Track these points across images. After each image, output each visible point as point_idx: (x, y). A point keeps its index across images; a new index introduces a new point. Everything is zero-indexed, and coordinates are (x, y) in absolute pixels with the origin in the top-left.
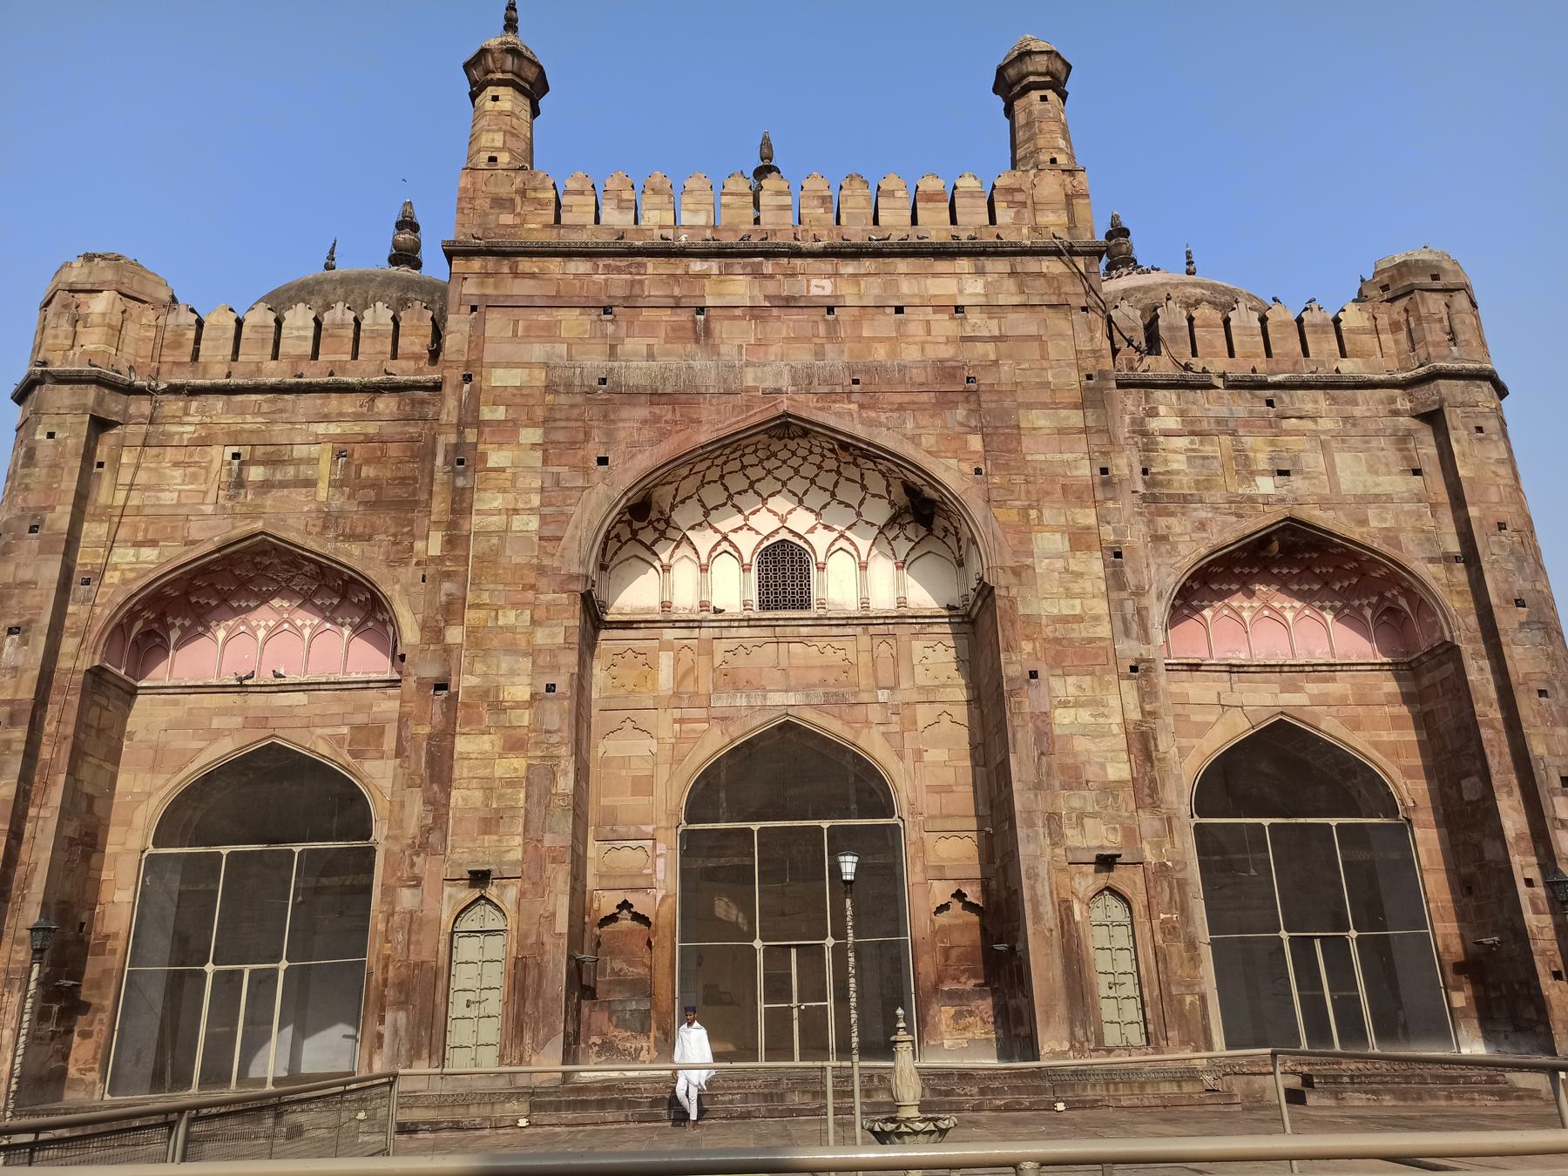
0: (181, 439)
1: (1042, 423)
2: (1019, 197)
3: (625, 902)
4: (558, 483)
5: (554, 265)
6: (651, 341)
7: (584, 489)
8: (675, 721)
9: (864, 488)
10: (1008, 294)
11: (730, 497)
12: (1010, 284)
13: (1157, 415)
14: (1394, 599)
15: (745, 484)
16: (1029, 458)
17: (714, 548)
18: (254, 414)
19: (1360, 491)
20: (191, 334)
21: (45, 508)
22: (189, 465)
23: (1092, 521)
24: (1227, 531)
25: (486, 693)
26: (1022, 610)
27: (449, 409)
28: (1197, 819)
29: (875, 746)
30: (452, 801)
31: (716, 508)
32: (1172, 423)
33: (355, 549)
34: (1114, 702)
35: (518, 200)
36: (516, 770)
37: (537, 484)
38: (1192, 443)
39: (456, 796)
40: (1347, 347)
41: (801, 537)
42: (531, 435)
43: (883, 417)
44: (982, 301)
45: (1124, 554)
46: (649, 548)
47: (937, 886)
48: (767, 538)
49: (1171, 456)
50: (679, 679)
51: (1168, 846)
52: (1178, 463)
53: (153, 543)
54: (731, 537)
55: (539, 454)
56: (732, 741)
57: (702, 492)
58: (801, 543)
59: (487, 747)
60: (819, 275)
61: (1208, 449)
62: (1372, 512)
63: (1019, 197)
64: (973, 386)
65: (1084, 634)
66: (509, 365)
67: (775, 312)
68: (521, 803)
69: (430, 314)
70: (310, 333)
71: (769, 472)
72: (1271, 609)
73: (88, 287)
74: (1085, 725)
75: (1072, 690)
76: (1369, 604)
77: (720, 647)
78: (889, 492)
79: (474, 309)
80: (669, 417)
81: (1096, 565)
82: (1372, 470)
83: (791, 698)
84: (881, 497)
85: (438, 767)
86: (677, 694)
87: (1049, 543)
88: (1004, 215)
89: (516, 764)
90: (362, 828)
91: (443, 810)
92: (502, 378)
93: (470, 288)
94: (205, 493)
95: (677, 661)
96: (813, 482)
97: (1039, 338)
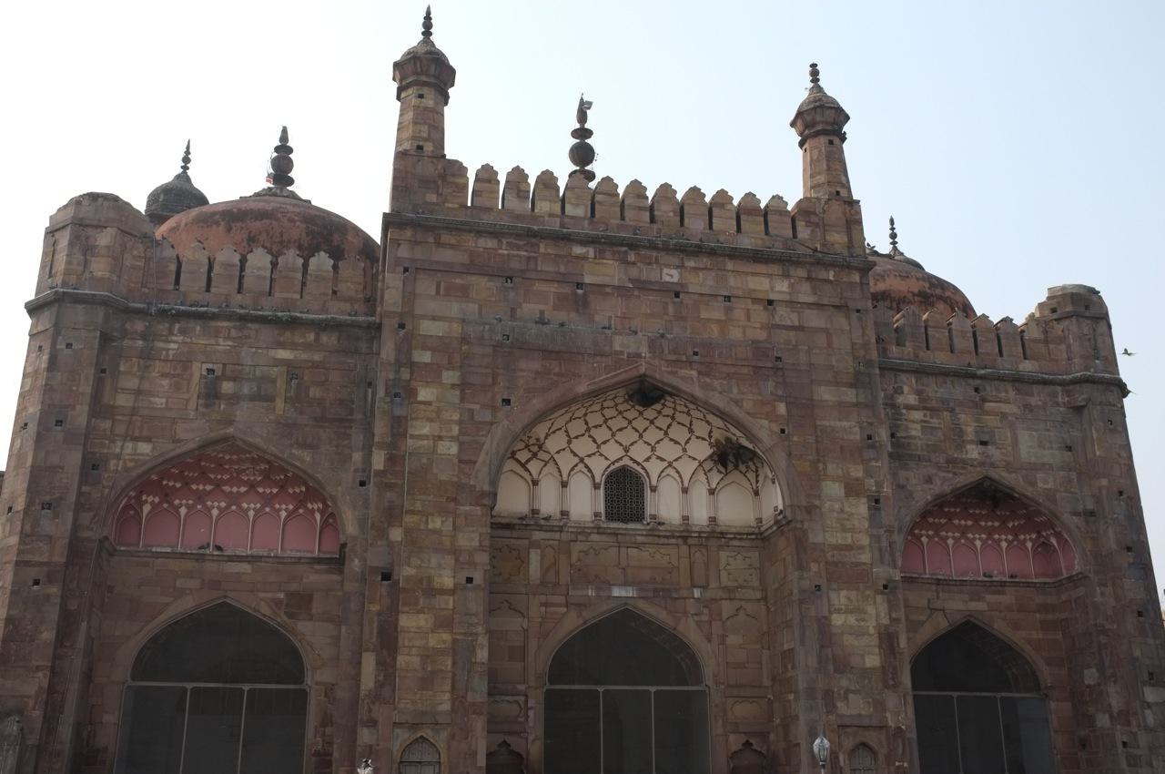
0: (167, 355)
1: (826, 397)
2: (814, 219)
4: (472, 417)
5: (471, 242)
6: (542, 307)
8: (542, 604)
9: (691, 431)
10: (806, 294)
11: (588, 430)
12: (806, 287)
13: (902, 393)
14: (1047, 538)
16: (818, 423)
17: (572, 469)
18: (225, 338)
19: (1033, 460)
20: (173, 267)
21: (67, 407)
22: (174, 376)
23: (860, 474)
24: (944, 483)
25: (421, 581)
27: (388, 349)
29: (691, 632)
30: (398, 663)
31: (576, 437)
32: (912, 399)
33: (307, 456)
34: (871, 610)
35: (440, 182)
36: (444, 642)
37: (456, 417)
38: (925, 415)
39: (401, 660)
40: (1028, 352)
42: (450, 377)
43: (716, 383)
44: (787, 297)
45: (881, 501)
46: (523, 465)
47: (732, 737)
50: (545, 572)
51: (903, 715)
52: (915, 431)
53: (148, 440)
54: (587, 460)
55: (457, 392)
56: (585, 623)
57: (569, 425)
58: (639, 469)
59: (422, 623)
60: (668, 266)
61: (935, 422)
62: (1040, 475)
63: (814, 219)
64: (780, 364)
65: (853, 560)
66: (434, 318)
67: (636, 293)
68: (449, 668)
71: (620, 413)
72: (967, 539)
73: (95, 223)
74: (851, 627)
75: (843, 600)
76: (1030, 539)
78: (710, 437)
79: (406, 270)
80: (557, 370)
81: (862, 508)
82: (1041, 446)
83: (629, 592)
84: (703, 439)
86: (543, 583)
87: (833, 489)
88: (804, 232)
90: (298, 676)
92: (429, 328)
93: (404, 252)
94: (187, 401)
95: (543, 556)
96: (652, 422)
97: (826, 331)
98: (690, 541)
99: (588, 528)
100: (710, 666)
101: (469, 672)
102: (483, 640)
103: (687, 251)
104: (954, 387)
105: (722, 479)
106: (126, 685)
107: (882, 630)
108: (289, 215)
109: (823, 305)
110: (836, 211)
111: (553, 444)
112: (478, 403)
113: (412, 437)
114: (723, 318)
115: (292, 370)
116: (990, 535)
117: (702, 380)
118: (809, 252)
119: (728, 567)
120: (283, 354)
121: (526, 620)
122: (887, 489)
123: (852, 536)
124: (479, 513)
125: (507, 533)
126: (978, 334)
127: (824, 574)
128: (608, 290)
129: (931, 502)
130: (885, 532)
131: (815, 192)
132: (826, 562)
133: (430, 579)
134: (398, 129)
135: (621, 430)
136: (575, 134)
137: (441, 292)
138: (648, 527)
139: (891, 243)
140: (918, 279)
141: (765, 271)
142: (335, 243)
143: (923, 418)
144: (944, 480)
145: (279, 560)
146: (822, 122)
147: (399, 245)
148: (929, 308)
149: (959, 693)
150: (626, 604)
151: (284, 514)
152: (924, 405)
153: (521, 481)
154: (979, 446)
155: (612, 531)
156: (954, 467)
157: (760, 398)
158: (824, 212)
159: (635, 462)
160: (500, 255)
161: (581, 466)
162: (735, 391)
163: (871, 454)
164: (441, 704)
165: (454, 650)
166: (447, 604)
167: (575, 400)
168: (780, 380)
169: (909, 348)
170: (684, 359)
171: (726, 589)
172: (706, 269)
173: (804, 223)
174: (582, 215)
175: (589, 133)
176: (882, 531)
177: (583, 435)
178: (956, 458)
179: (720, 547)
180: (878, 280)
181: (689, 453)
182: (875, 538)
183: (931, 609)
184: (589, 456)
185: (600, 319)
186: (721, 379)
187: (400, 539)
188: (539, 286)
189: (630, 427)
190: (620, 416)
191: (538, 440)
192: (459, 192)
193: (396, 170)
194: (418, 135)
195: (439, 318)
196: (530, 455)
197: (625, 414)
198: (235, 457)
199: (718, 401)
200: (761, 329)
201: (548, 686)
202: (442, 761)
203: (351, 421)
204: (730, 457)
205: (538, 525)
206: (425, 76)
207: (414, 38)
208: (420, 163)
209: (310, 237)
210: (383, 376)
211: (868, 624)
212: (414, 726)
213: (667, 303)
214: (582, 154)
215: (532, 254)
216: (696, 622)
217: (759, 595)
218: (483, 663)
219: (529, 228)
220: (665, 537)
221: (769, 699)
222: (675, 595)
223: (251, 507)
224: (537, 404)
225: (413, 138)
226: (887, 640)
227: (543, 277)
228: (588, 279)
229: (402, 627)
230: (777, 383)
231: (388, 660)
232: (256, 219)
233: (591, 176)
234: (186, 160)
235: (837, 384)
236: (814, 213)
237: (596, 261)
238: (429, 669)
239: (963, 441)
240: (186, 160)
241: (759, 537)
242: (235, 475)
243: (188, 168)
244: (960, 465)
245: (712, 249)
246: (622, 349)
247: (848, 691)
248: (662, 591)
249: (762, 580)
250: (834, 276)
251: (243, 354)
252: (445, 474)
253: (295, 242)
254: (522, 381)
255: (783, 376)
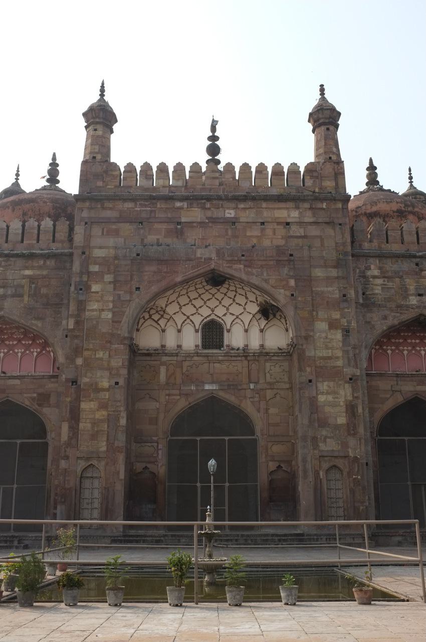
1: (319, 274)
2: (315, 174)
3: (146, 467)
6: (158, 237)
7: (130, 301)
8: (167, 395)
9: (247, 298)
10: (309, 217)
11: (191, 301)
13: (370, 269)
15: (197, 295)
17: (183, 322)
24: (394, 319)
25: (92, 385)
26: (307, 354)
27: (76, 266)
28: (379, 438)
29: (248, 407)
30: (80, 427)
31: (184, 305)
32: (376, 272)
33: (39, 324)
34: (342, 392)
35: (105, 175)
36: (104, 416)
37: (111, 299)
38: (384, 281)
39: (81, 425)
41: (220, 318)
42: (108, 278)
43: (254, 271)
44: (297, 220)
46: (156, 322)
47: (271, 464)
48: (206, 318)
49: (375, 287)
50: (168, 378)
51: (359, 450)
52: (378, 290)
54: (191, 317)
55: (112, 286)
56: (190, 404)
58: (220, 320)
60: (228, 208)
61: (390, 284)
63: (315, 174)
64: (292, 258)
65: (332, 365)
66: (100, 248)
67: (210, 225)
68: (106, 429)
69: (68, 222)
70: (20, 232)
71: (207, 291)
74: (330, 402)
75: (325, 387)
77: (186, 364)
78: (257, 301)
79: (86, 223)
80: (165, 270)
81: (338, 335)
84: (254, 302)
85: (75, 416)
86: (167, 384)
87: (322, 326)
89: (102, 414)
91: (76, 431)
92: (98, 253)
93: (85, 214)
95: (167, 370)
96: (225, 295)
97: (320, 237)
98: (249, 358)
99: (257, 353)
100: (259, 425)
101: (116, 431)
102: (124, 415)
103: (237, 199)
104: (403, 264)
105: (267, 323)
106: (168, 439)
107: (348, 403)
108: (43, 200)
109: (319, 223)
110: (329, 169)
111: (171, 310)
112: (122, 291)
113: (89, 310)
114: (259, 235)
115: (32, 279)
116: (414, 347)
117: (246, 270)
118: (311, 193)
119: (270, 372)
120: (28, 272)
121: (158, 403)
122: (354, 324)
123: (332, 351)
124: (123, 348)
125: (148, 358)
126: (419, 232)
127: (314, 373)
128: (195, 224)
129: (386, 331)
130: (352, 348)
131: (318, 159)
132: (316, 367)
133: (96, 384)
134: (85, 149)
135: (209, 300)
136: (210, 138)
137: (105, 233)
138: (225, 352)
139: (409, 182)
140: (397, 203)
141: (285, 207)
142: (69, 212)
143: (383, 283)
144: (394, 317)
145: (34, 377)
146: (323, 118)
147: (82, 210)
148: (403, 219)
149: (409, 438)
150: (212, 393)
151: (35, 354)
152: (384, 275)
153: (157, 331)
154: (418, 297)
155: (205, 355)
156: (400, 310)
157: (279, 277)
158: (321, 169)
159: (218, 317)
160: (135, 211)
161: (188, 321)
162: (265, 275)
163: (345, 305)
164: (102, 447)
165: (108, 419)
166: (105, 396)
167: (175, 285)
168: (292, 267)
169: (375, 243)
170: (236, 259)
171: (270, 383)
172: (250, 208)
173: (309, 177)
174: (181, 185)
175: (217, 138)
176: (350, 348)
177: (188, 304)
178: (403, 305)
179: (266, 361)
180: (373, 205)
181: (247, 310)
182: (346, 352)
183: (393, 391)
184: (192, 315)
185: (190, 241)
186: (257, 268)
187: (81, 364)
188: (156, 226)
189: (214, 298)
190: (207, 293)
191: (162, 308)
192: (114, 179)
193: (81, 171)
194: (93, 151)
195: (104, 247)
196: (160, 316)
197: (198, 290)
198: (8, 326)
199: (255, 280)
200: (282, 239)
201: (170, 437)
202: (102, 476)
203: (61, 304)
204: (268, 312)
205: (165, 353)
206: (101, 118)
207: (95, 98)
208: (94, 166)
209: (55, 210)
210: (75, 279)
211: (340, 400)
212: (88, 459)
213: (227, 229)
214: (214, 150)
215: (153, 209)
216: (251, 402)
217: (288, 386)
218: (123, 426)
219: (151, 195)
220: (234, 356)
221: (293, 443)
222: (240, 388)
223: (19, 351)
224: (154, 289)
225: (91, 153)
226: (351, 409)
227: (159, 221)
228: (183, 220)
229: (82, 409)
230: (291, 268)
231: (75, 426)
232: (27, 203)
233: (218, 162)
234: (17, 175)
235: (326, 266)
236: (316, 171)
237: (188, 209)
238: (96, 430)
239: (408, 295)
240: (17, 175)
241: (288, 354)
242: (10, 335)
243: (18, 179)
244: (405, 308)
245: (253, 197)
246: (201, 256)
247: (326, 437)
248: (232, 385)
249: (290, 378)
250: (326, 206)
251: (8, 274)
252: (104, 329)
253: (46, 213)
254: (146, 277)
255: (294, 264)
